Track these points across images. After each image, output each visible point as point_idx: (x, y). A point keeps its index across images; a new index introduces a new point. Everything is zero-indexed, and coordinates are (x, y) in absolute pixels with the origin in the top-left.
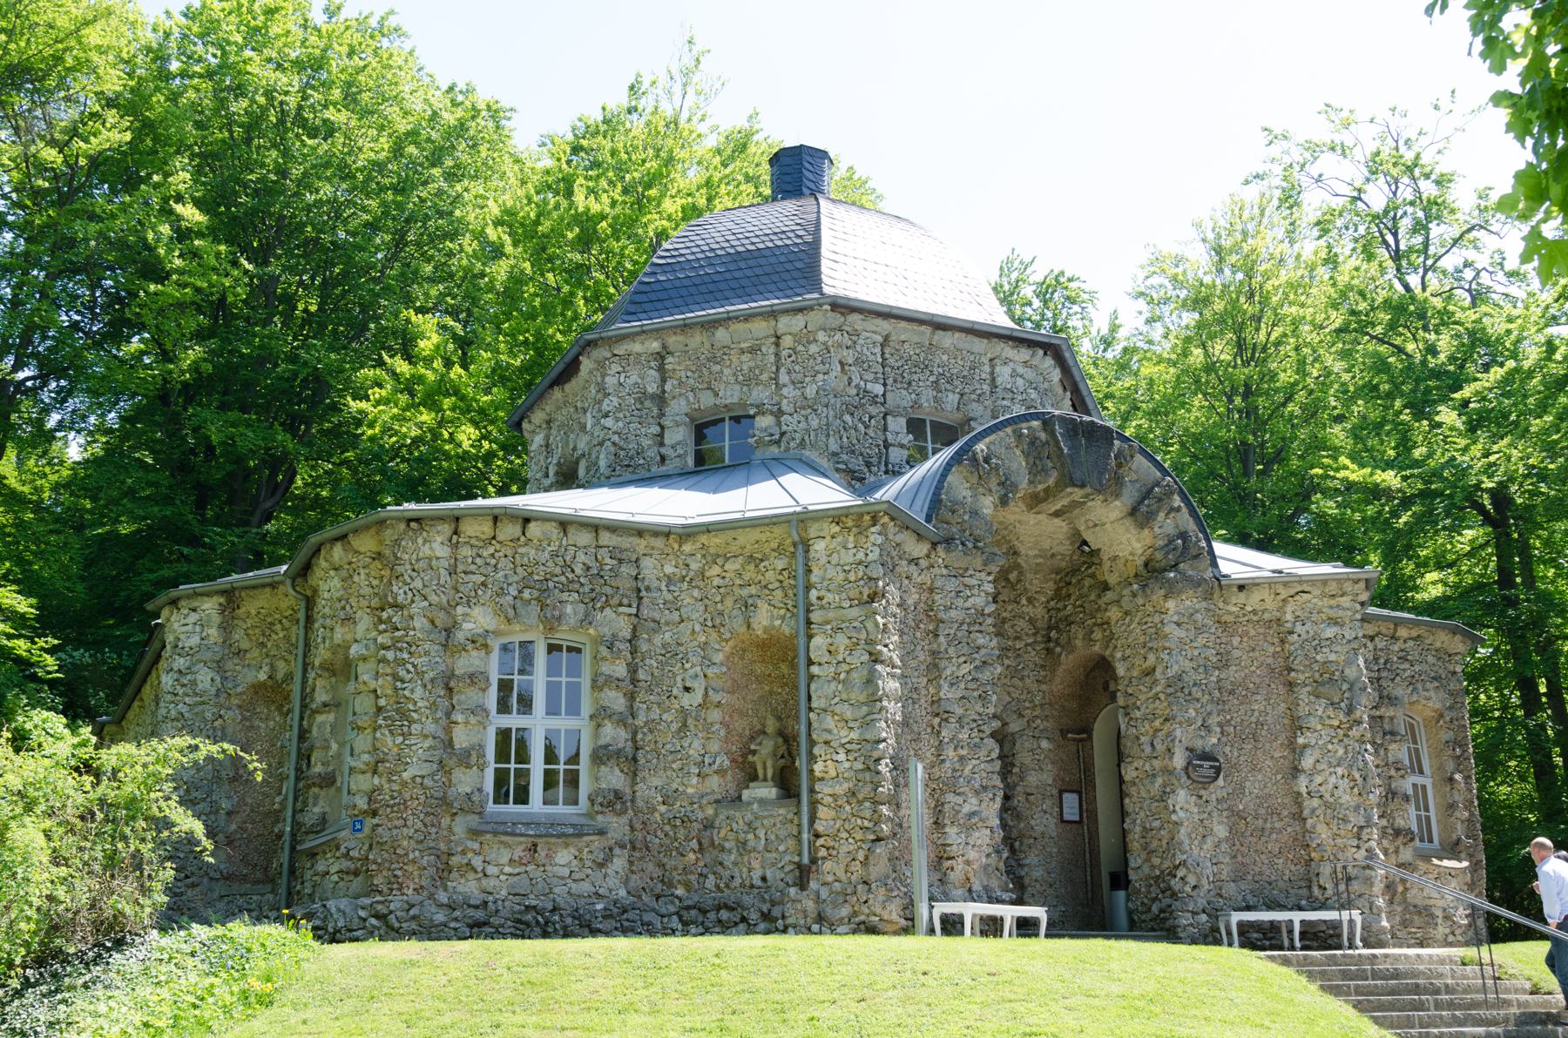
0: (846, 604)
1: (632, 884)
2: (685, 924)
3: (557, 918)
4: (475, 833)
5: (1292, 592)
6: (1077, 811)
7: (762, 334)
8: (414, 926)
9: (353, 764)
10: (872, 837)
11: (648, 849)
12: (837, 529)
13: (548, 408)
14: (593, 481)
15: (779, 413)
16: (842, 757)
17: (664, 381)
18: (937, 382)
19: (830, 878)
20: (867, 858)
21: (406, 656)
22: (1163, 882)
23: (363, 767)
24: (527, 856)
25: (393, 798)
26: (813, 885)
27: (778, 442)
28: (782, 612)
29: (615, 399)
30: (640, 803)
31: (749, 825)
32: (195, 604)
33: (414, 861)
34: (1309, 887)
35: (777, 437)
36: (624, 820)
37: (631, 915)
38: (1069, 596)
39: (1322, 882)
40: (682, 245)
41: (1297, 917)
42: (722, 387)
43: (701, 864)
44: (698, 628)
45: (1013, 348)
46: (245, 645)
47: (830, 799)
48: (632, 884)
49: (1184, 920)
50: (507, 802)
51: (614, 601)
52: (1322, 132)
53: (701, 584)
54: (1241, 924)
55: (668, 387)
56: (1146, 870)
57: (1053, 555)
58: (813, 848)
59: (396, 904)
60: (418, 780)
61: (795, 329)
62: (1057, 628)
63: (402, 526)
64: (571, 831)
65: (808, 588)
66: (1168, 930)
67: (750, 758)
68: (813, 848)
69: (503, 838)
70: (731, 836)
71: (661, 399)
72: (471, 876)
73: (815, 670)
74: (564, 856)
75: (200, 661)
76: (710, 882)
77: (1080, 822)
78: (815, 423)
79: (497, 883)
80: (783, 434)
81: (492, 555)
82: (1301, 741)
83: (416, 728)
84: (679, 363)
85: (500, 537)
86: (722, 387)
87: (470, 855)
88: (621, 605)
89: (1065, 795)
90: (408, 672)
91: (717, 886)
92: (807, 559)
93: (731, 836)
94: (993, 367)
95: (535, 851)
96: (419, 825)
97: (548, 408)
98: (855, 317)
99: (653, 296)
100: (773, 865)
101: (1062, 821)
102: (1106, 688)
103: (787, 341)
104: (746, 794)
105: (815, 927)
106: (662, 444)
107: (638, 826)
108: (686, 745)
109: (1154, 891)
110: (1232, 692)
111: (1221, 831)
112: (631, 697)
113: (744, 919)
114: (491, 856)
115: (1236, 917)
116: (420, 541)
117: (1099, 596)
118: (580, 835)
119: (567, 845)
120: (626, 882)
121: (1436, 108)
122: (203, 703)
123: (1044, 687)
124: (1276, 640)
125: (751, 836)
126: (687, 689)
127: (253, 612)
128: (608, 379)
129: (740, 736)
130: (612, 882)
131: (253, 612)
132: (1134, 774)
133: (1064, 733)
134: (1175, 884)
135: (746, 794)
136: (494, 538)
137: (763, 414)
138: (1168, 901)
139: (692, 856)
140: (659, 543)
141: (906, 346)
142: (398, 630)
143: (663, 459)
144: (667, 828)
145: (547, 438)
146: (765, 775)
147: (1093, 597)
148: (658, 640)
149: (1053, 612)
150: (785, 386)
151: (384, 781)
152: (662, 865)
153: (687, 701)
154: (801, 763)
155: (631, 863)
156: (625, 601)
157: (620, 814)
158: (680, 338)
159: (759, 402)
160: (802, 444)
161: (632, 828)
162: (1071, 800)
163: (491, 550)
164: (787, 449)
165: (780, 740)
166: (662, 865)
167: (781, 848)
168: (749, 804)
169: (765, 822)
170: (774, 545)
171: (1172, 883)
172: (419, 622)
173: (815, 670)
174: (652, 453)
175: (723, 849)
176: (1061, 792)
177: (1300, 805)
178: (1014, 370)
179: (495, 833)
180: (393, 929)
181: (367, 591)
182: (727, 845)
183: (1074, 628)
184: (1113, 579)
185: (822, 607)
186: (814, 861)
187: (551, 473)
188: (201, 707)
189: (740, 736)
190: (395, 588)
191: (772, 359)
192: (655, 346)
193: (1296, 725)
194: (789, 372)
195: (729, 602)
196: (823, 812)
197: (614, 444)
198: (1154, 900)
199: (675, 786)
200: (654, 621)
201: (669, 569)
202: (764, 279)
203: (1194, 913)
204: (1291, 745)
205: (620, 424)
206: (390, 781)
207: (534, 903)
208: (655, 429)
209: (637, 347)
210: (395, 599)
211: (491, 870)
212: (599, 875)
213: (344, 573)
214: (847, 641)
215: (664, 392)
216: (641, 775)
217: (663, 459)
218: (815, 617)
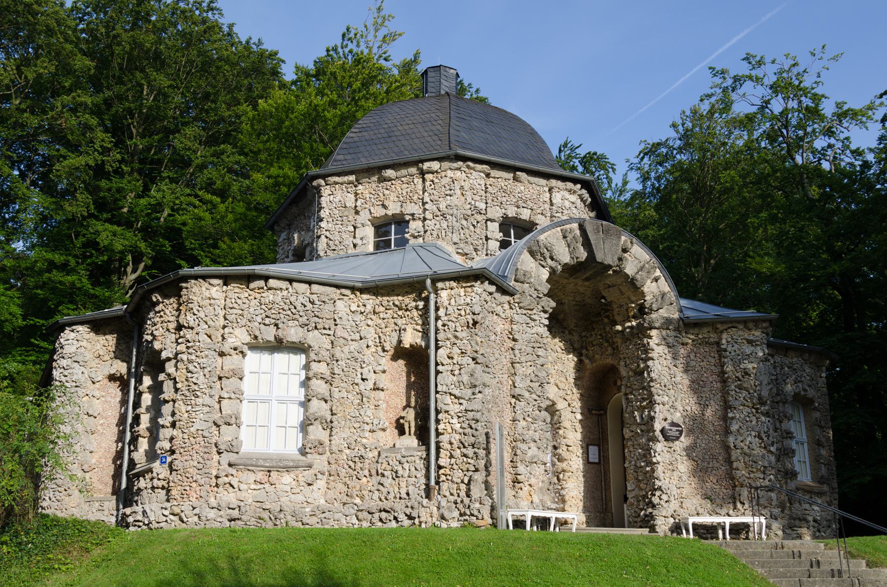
1: (328, 496)
6: (597, 456)
43: (371, 484)
52: (743, 69)
65: (437, 318)
67: (402, 421)
73: (440, 368)
77: (599, 463)
82: (730, 415)
101: (589, 463)
108: (362, 413)
116: (203, 289)
124: (716, 355)
134: (655, 500)
143: (355, 246)
148: (346, 349)
150: (427, 203)
162: (594, 450)
168: (400, 449)
175: (383, 475)
176: (588, 446)
196: (443, 453)
197: (327, 237)
198: (641, 510)
201: (354, 307)
205: (330, 225)
218: (441, 336)
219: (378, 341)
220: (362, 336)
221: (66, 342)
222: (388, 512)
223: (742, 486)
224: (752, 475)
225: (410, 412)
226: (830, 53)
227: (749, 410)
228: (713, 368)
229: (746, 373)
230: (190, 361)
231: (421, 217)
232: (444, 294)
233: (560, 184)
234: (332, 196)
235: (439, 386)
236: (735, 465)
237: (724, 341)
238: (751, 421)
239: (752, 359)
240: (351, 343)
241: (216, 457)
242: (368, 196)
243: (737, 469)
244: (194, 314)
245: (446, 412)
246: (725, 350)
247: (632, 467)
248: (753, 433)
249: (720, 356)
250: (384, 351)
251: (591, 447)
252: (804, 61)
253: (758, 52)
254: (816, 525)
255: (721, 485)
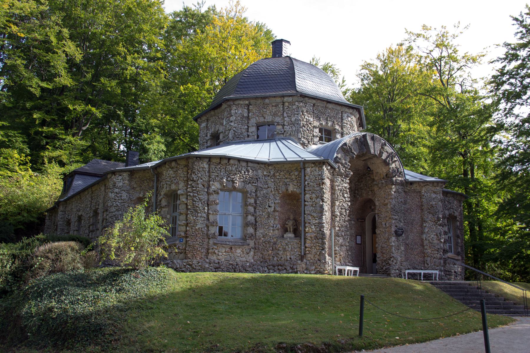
0: (316, 186)
1: (255, 259)
2: (269, 269)
3: (238, 267)
4: (215, 244)
5: (424, 185)
6: (360, 241)
7: (279, 101)
8: (199, 268)
9: (180, 223)
10: (321, 249)
11: (259, 249)
12: (313, 165)
13: (208, 116)
14: (228, 143)
15: (283, 125)
16: (313, 227)
17: (249, 113)
18: (327, 118)
19: (309, 259)
20: (320, 254)
21: (196, 195)
22: (387, 262)
23: (183, 224)
24: (229, 250)
25: (193, 233)
26: (305, 260)
27: (283, 134)
28: (296, 187)
29: (234, 117)
30: (257, 237)
31: (286, 244)
32: (121, 174)
33: (199, 251)
34: (424, 264)
35: (283, 132)
36: (253, 241)
37: (255, 267)
38: (362, 182)
39: (428, 262)
40: (251, 71)
41: (422, 272)
42: (267, 116)
43: (273, 254)
44: (273, 190)
45: (348, 109)
46: (135, 186)
47: (310, 238)
48: (255, 259)
49: (393, 272)
50: (424, 273)
51: (251, 182)
52: (419, 30)
53: (273, 178)
54: (408, 273)
55: (250, 115)
56: (382, 258)
57: (358, 170)
58: (305, 251)
59: (195, 262)
60: (200, 229)
61: (289, 101)
62: (358, 190)
63: (195, 159)
64: (241, 244)
65: (305, 180)
66: (388, 274)
67: (286, 226)
68: (305, 251)
69: (223, 245)
70: (281, 247)
71: (248, 118)
72: (215, 255)
73: (306, 203)
74: (239, 251)
75: (123, 190)
76: (275, 259)
77: (361, 244)
78: (294, 129)
79: (221, 257)
80: (285, 131)
81: (220, 168)
82: (424, 225)
83: (199, 215)
84: (253, 108)
85: (222, 163)
86: (267, 116)
87: (214, 249)
88: (253, 183)
89: (357, 237)
90: (197, 199)
91: (277, 260)
92: (305, 173)
93: (281, 247)
94: (342, 114)
95: (232, 249)
96: (201, 241)
97: (208, 116)
98: (306, 99)
99: (244, 86)
100: (293, 255)
101: (357, 244)
102: (371, 207)
103: (287, 104)
104: (285, 236)
105: (305, 272)
106: (248, 131)
107: (257, 243)
108: (269, 222)
109: (384, 264)
110: (407, 211)
111: (403, 248)
112: (255, 208)
113: (285, 269)
114: (220, 250)
115: (407, 271)
116: (200, 163)
117: (372, 183)
118: (243, 245)
119: (239, 248)
120: (253, 258)
121: (455, 26)
122: (124, 202)
123: (353, 206)
124: (419, 197)
125: (287, 247)
126: (269, 206)
127: (137, 177)
128: (232, 111)
129: (282, 219)
130: (251, 258)
131: (137, 177)
132: (380, 232)
133: (358, 220)
134: (390, 262)
135: (285, 236)
136: (220, 163)
137: (279, 125)
138: (388, 267)
139: (270, 252)
140: (263, 166)
141: (319, 107)
142: (193, 187)
143: (248, 136)
144: (264, 244)
145: (207, 125)
146: (290, 231)
147: (370, 183)
148: (262, 193)
149: (357, 186)
150: (285, 117)
151: (190, 228)
152: (262, 254)
153: (269, 210)
154: (301, 228)
155: (255, 253)
156: (254, 182)
157: (252, 240)
158: (254, 101)
159: (277, 121)
160: (290, 135)
161: (255, 244)
162: (359, 238)
163: (219, 167)
164: (286, 136)
165: (294, 221)
166: (262, 254)
167: (295, 250)
168: (286, 238)
169: (291, 243)
170: (295, 168)
171: (390, 261)
172: (200, 186)
173: (306, 203)
174: (245, 134)
175: (279, 250)
176: (356, 236)
177: (423, 242)
178: (348, 115)
179: (221, 244)
180: (193, 268)
181: (182, 175)
182: (280, 249)
183: (363, 191)
184: (376, 178)
185: (309, 186)
186: (305, 254)
187: (208, 136)
188: (124, 203)
189: (282, 219)
190: (193, 176)
191: (282, 109)
192: (247, 102)
193: (423, 221)
194: (287, 113)
195: (281, 184)
196: (308, 241)
197: (234, 130)
198: (384, 266)
199: (266, 233)
200: (261, 187)
201: (265, 173)
202: (278, 84)
203: (395, 270)
204: (421, 226)
205: (236, 125)
206: (192, 229)
207: (232, 263)
208: (246, 127)
209: (241, 102)
210: (193, 179)
211: (220, 254)
212: (247, 256)
213: (175, 170)
214: (315, 196)
215: (249, 116)
216: (257, 229)
217: (248, 136)
218: (307, 189)
219: (275, 189)
220: (269, 186)
221: (117, 181)
222: (282, 266)
223: (428, 256)
224: (432, 252)
225: (290, 222)
226: (462, 26)
227: (433, 223)
228: (417, 203)
229: (432, 206)
230: (194, 196)
231: (283, 124)
232: (308, 170)
233: (347, 110)
234: (237, 110)
235: (306, 211)
236: (425, 247)
237: (423, 191)
238: (433, 228)
239: (435, 200)
240: (264, 189)
241: (207, 240)
242: (255, 111)
243: (426, 249)
244: (196, 175)
245: (309, 223)
246: (423, 195)
247: (380, 247)
248: (434, 234)
249: (421, 198)
250: (279, 193)
251: (358, 237)
252: (451, 31)
253: (428, 25)
254: (455, 274)
255: (418, 256)
